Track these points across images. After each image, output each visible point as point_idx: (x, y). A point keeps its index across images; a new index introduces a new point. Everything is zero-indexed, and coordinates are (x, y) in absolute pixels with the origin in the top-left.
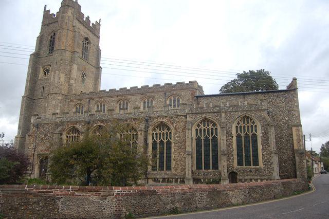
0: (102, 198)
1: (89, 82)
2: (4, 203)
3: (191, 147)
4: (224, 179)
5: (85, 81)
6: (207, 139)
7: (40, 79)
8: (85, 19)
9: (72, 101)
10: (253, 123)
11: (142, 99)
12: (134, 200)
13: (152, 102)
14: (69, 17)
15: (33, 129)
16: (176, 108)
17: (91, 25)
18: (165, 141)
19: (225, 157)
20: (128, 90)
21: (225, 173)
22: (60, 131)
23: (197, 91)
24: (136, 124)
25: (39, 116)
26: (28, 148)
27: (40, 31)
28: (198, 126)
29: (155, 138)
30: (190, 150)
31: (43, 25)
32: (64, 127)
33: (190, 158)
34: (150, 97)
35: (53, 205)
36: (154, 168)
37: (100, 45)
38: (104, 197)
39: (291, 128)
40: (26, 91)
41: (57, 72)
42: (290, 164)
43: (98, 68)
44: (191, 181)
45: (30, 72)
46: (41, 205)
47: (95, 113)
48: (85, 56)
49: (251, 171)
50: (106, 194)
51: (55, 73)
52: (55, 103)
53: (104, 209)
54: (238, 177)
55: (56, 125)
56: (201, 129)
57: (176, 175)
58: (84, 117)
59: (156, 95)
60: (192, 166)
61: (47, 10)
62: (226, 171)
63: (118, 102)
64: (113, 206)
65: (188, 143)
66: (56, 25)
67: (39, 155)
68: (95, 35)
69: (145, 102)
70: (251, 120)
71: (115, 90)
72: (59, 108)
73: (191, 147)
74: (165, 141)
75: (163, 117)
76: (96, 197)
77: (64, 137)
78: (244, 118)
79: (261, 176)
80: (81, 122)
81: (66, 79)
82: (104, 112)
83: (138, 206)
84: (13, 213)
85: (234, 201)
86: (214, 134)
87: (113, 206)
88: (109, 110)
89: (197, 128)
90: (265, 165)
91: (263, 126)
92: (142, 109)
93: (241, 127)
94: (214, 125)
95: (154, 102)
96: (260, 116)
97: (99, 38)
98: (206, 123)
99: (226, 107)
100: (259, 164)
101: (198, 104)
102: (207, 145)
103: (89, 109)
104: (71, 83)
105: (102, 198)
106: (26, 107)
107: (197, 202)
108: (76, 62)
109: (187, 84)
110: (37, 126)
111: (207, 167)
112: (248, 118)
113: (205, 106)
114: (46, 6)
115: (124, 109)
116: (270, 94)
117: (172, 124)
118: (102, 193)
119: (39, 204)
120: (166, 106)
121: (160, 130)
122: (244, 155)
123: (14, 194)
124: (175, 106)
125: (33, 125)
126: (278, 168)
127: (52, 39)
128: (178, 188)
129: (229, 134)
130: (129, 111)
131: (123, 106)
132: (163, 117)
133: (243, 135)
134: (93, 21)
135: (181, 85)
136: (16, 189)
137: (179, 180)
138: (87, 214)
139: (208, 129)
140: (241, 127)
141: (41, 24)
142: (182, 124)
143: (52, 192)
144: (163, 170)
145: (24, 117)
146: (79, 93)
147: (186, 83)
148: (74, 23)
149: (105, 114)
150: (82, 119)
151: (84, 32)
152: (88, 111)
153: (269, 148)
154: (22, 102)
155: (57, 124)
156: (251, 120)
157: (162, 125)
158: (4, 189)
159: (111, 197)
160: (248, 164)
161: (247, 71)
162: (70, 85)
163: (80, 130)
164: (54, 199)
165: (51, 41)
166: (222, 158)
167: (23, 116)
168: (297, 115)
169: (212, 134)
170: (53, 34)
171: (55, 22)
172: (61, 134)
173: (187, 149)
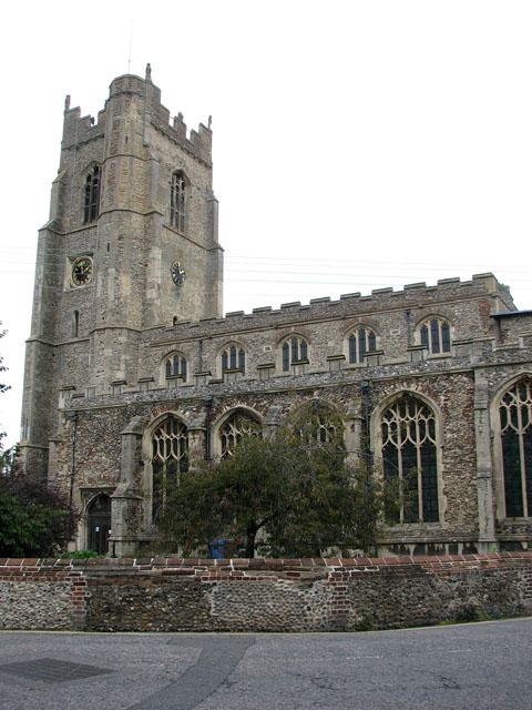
1: (193, 290)
3: (489, 456)
8: (171, 123)
9: (156, 345)
12: (372, 588)
14: (132, 125)
15: (63, 426)
16: (442, 354)
17: (188, 136)
18: (418, 444)
20: (306, 309)
22: (136, 428)
23: (497, 301)
27: (57, 166)
28: (507, 398)
30: (489, 465)
31: (67, 148)
32: (146, 418)
33: (489, 488)
35: (198, 601)
37: (214, 188)
38: (307, 583)
43: (214, 250)
46: (170, 600)
48: (178, 221)
50: (312, 574)
53: (309, 609)
55: (124, 413)
56: (514, 409)
58: (192, 385)
60: (495, 506)
61: (71, 107)
64: (328, 603)
65: (482, 446)
66: (98, 144)
67: (85, 492)
68: (200, 161)
72: (123, 366)
73: (489, 457)
74: (418, 444)
75: (408, 379)
76: (288, 582)
80: (187, 402)
84: (114, 618)
89: (504, 404)
98: (528, 389)
101: (502, 337)
104: (149, 297)
106: (37, 367)
107: (521, 594)
108: (157, 240)
109: (468, 284)
110: (76, 417)
115: (233, 370)
117: (435, 396)
118: (303, 575)
119: (166, 599)
121: (403, 415)
123: (112, 577)
127: (91, 184)
128: (473, 564)
130: (247, 377)
131: (176, 370)
132: (408, 379)
134: (192, 124)
136: (114, 568)
137: (461, 547)
138: (271, 620)
141: (59, 147)
142: (463, 397)
143: (193, 573)
147: (428, 285)
148: (146, 136)
150: (189, 394)
151: (170, 155)
154: (28, 356)
157: (408, 402)
158: (88, 568)
162: (146, 304)
163: (190, 425)
164: (198, 588)
165: (88, 189)
171: (95, 140)
172: (140, 437)
173: (479, 464)
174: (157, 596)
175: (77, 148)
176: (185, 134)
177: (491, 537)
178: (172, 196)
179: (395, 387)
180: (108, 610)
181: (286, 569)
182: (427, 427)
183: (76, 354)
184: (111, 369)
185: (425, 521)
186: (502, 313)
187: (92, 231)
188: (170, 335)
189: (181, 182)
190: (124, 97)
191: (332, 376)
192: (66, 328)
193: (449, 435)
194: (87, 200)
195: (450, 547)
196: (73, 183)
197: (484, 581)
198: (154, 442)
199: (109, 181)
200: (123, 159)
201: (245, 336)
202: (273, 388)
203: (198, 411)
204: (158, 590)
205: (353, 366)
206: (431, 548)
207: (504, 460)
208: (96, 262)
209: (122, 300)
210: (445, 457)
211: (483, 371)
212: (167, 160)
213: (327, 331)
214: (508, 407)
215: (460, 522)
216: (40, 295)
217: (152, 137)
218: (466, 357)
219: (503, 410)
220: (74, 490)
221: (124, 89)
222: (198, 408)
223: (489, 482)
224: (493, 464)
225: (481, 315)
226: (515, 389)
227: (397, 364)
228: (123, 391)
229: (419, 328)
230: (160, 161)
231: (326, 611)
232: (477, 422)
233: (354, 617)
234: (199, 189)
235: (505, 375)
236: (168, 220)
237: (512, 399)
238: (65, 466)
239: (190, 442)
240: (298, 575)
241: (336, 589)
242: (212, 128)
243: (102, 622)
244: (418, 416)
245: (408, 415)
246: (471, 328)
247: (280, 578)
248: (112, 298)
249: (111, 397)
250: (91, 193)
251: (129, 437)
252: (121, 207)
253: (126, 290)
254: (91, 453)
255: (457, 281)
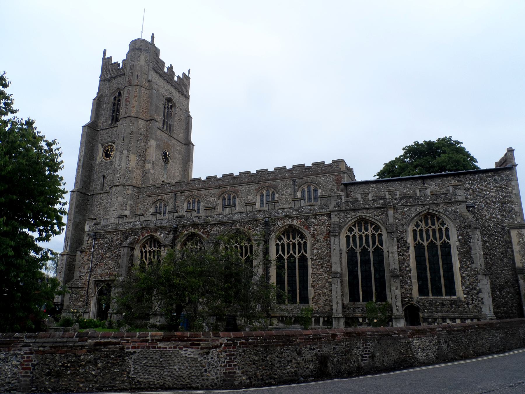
0: (201, 352)
2: (37, 364)
4: (398, 318)
5: (169, 165)
6: (365, 252)
7: (99, 164)
8: (166, 70)
9: (149, 196)
10: (443, 224)
11: (258, 190)
12: (255, 354)
13: (273, 194)
15: (87, 241)
18: (297, 256)
19: (398, 281)
20: (236, 177)
21: (398, 308)
22: (131, 243)
24: (249, 229)
25: (98, 221)
26: (80, 272)
28: (350, 230)
29: (280, 252)
30: (339, 270)
31: (103, 79)
32: (137, 237)
34: (269, 187)
35: (121, 366)
36: (280, 300)
38: (205, 351)
39: (509, 232)
40: (76, 182)
41: (125, 152)
42: (509, 292)
43: (188, 145)
44: (342, 322)
45: (83, 154)
46: (99, 365)
47: (185, 214)
49: (442, 305)
51: (122, 154)
52: (121, 200)
54: (421, 315)
56: (354, 236)
57: (317, 312)
58: (169, 220)
59: (279, 184)
60: (342, 295)
61: (106, 57)
62: (399, 304)
63: (220, 196)
64: (221, 366)
65: (335, 259)
66: (122, 79)
67: (97, 282)
68: (182, 94)
69: (262, 195)
70: (438, 219)
71: (215, 177)
72: (129, 208)
73: (339, 265)
75: (292, 217)
76: (192, 350)
77: (137, 253)
78: (426, 216)
79: (461, 313)
80: (163, 228)
81: (140, 163)
82: (199, 212)
83: (261, 365)
84: (53, 380)
85: (420, 356)
86: (377, 243)
87: (221, 366)
88: (207, 209)
89: (349, 234)
90: (467, 294)
91: (459, 229)
92: (258, 204)
93: (421, 231)
94: (377, 228)
95: (277, 195)
96: (455, 212)
97: (189, 98)
98: (363, 225)
99: (396, 199)
100: (457, 294)
102: (365, 262)
103: (175, 208)
104: (147, 168)
105: (201, 352)
108: (154, 136)
109: (329, 165)
110: (95, 236)
111: (367, 297)
112: (433, 216)
113: (360, 199)
114: (105, 53)
115: (229, 206)
116: (468, 176)
117: (308, 228)
118: (202, 344)
119: (96, 364)
120: (296, 200)
122: (429, 277)
124: (309, 199)
125: (89, 236)
126: (491, 299)
127: (116, 102)
129: (402, 244)
132: (292, 217)
133: (425, 243)
134: (178, 72)
135: (318, 166)
136: (59, 340)
137: (322, 320)
139: (367, 236)
140: (421, 231)
142: (324, 228)
144: (295, 303)
145: (73, 223)
146: (159, 183)
149: (201, 214)
150: (164, 224)
152: (175, 211)
153: (474, 266)
155: (125, 233)
156: (438, 219)
158: (37, 340)
159: (218, 350)
160: (437, 292)
161: (421, 142)
162: (145, 172)
163: (162, 242)
165: (114, 104)
166: (393, 282)
167: (72, 221)
168: (517, 209)
169: (374, 243)
170: (118, 94)
172: (133, 249)
174: (90, 362)
175: (109, 81)
176: (174, 78)
177: (340, 315)
178: (164, 112)
179: (284, 222)
180: (49, 374)
181: (190, 340)
182: (302, 246)
183: (101, 199)
184: (122, 209)
185: (301, 303)
186: (348, 182)
187: (115, 129)
188: (158, 191)
189: (170, 104)
190: (137, 52)
191: (248, 214)
192: (97, 185)
193: (315, 251)
194: (113, 111)
195: (315, 320)
196: (105, 101)
197: (334, 348)
198: (142, 252)
199: (126, 100)
200: (135, 87)
201: (201, 192)
202: (212, 221)
203: (168, 234)
204: (91, 357)
205: (261, 209)
206: (303, 321)
207: (348, 267)
208: (117, 146)
209: (130, 169)
210: (313, 264)
211: (336, 213)
212: (162, 91)
213: (248, 190)
214: (351, 236)
215: (322, 304)
216: (81, 165)
217: (153, 76)
218: (326, 205)
219: (348, 237)
220: (90, 281)
221: (137, 46)
222: (169, 232)
223: (339, 280)
224: (341, 270)
225: (336, 183)
226: (355, 224)
227: (286, 208)
228: (124, 221)
229: (300, 190)
230: (158, 91)
231: (219, 372)
232: (332, 244)
233: (240, 376)
234: (181, 110)
235: (349, 216)
236: (161, 126)
237: (353, 230)
238: (86, 267)
239: (162, 252)
240: (199, 345)
241: (227, 355)
242: (190, 76)
243: (43, 383)
244: (297, 240)
245: (291, 239)
246: (330, 190)
247: (185, 347)
248: (124, 166)
249: (117, 225)
250: (116, 107)
251: (126, 249)
252: (132, 115)
253: (133, 163)
254: (102, 258)
255: (323, 163)
